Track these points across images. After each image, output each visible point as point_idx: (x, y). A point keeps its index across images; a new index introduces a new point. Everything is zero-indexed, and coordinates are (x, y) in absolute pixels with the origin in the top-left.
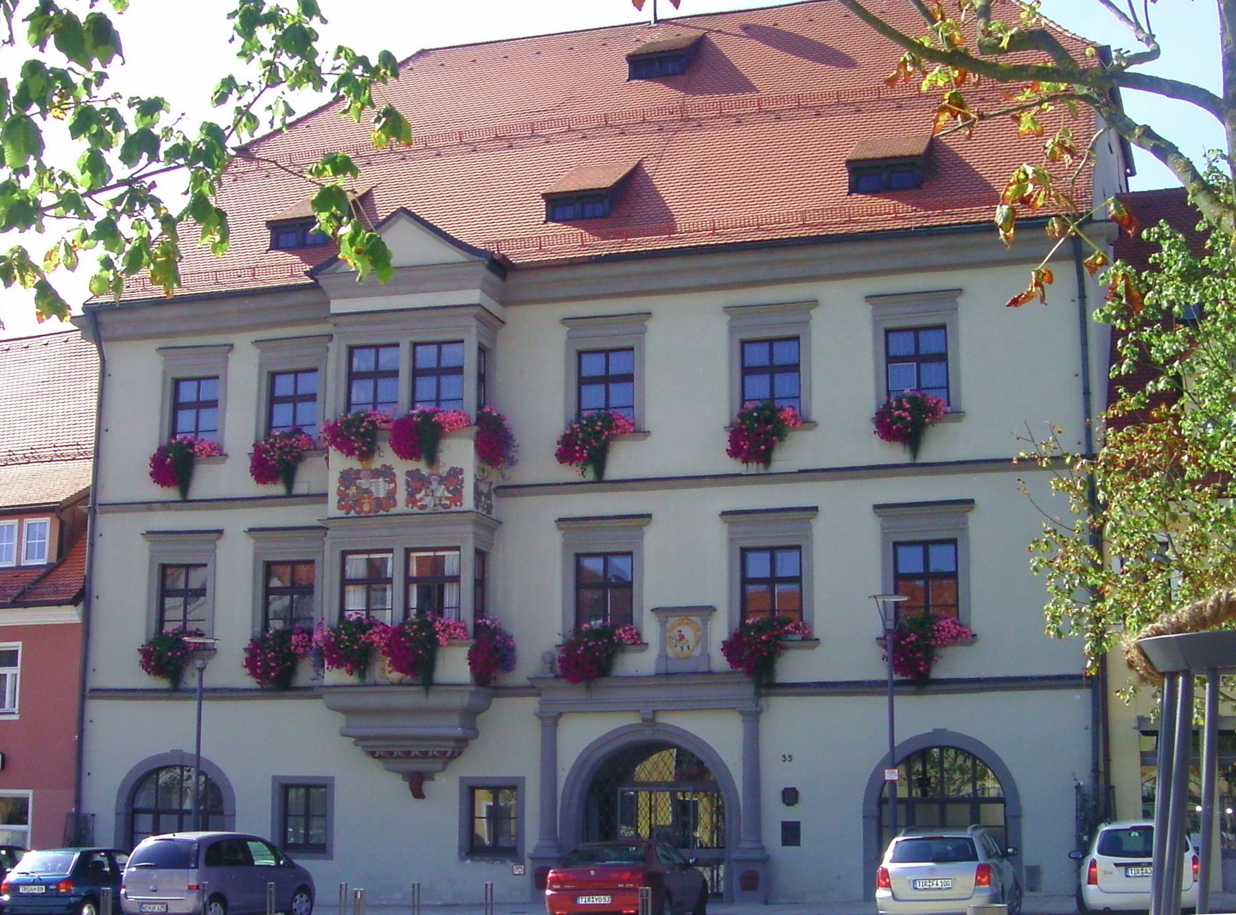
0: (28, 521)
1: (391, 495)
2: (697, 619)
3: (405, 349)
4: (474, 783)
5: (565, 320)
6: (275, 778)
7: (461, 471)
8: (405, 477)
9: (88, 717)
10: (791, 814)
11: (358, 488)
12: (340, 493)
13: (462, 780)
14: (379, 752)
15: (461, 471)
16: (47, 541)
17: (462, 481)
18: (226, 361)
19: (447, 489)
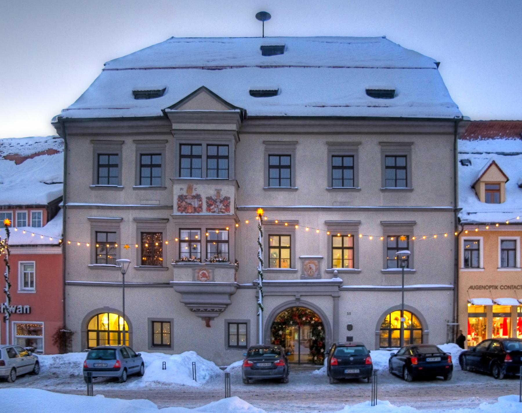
0: (32, 211)
1: (200, 207)
2: (316, 261)
3: (204, 146)
4: (248, 324)
5: (264, 142)
6: (149, 319)
7: (229, 198)
8: (205, 200)
9: (66, 293)
10: (350, 334)
11: (186, 203)
12: (178, 204)
13: (225, 320)
14: (194, 309)
15: (229, 198)
16: (42, 220)
17: (230, 203)
18: (122, 148)
19: (224, 205)
